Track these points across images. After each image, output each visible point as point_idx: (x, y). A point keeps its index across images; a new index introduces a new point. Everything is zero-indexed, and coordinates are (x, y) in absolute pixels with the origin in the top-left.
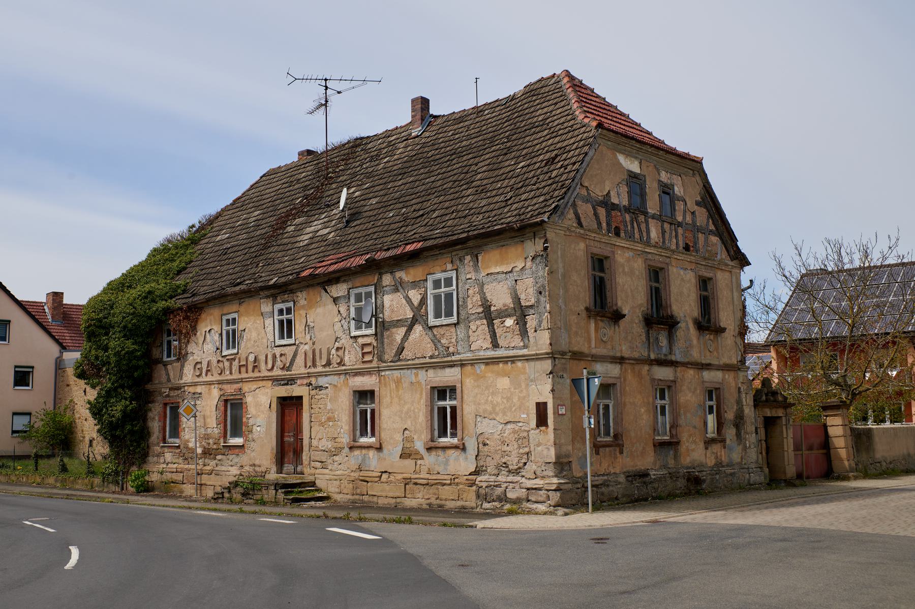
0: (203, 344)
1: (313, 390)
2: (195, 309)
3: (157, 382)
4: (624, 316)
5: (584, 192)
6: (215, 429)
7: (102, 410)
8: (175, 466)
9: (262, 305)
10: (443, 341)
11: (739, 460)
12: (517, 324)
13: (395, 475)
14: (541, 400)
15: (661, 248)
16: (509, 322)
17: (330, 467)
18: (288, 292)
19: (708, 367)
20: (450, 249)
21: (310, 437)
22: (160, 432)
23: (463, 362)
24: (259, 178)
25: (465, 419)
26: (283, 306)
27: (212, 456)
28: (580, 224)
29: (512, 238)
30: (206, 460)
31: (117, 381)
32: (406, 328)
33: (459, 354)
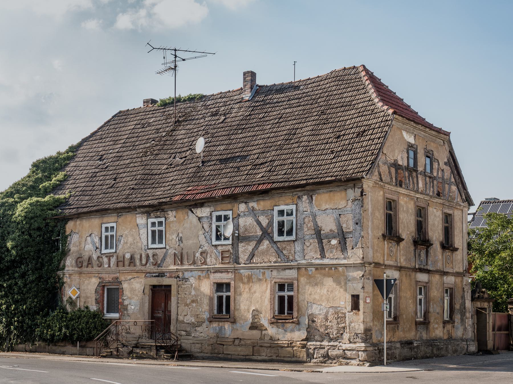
1: (180, 281)
4: (403, 240)
5: (384, 157)
9: (137, 219)
10: (285, 252)
11: (461, 336)
12: (340, 243)
13: (245, 340)
14: (355, 293)
15: (424, 194)
16: (334, 242)
17: (193, 335)
18: (160, 211)
19: (445, 273)
20: (293, 190)
21: (177, 314)
23: (300, 267)
24: (111, 117)
25: (300, 304)
26: (156, 220)
28: (381, 180)
29: (338, 186)
32: (256, 242)
33: (296, 261)
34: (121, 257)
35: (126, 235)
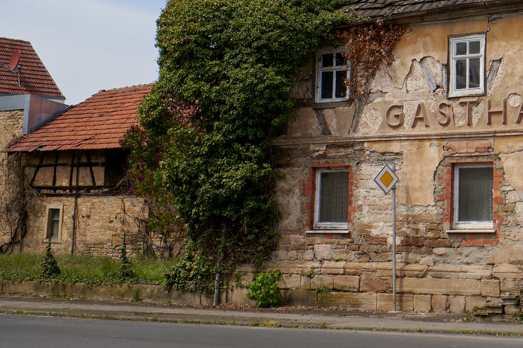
0: (406, 78)
2: (393, 26)
3: (299, 134)
6: (429, 208)
7: (196, 177)
8: (341, 264)
22: (303, 211)
27: (423, 249)
30: (411, 256)
31: (234, 131)
34: (498, 105)
35: (512, 60)
